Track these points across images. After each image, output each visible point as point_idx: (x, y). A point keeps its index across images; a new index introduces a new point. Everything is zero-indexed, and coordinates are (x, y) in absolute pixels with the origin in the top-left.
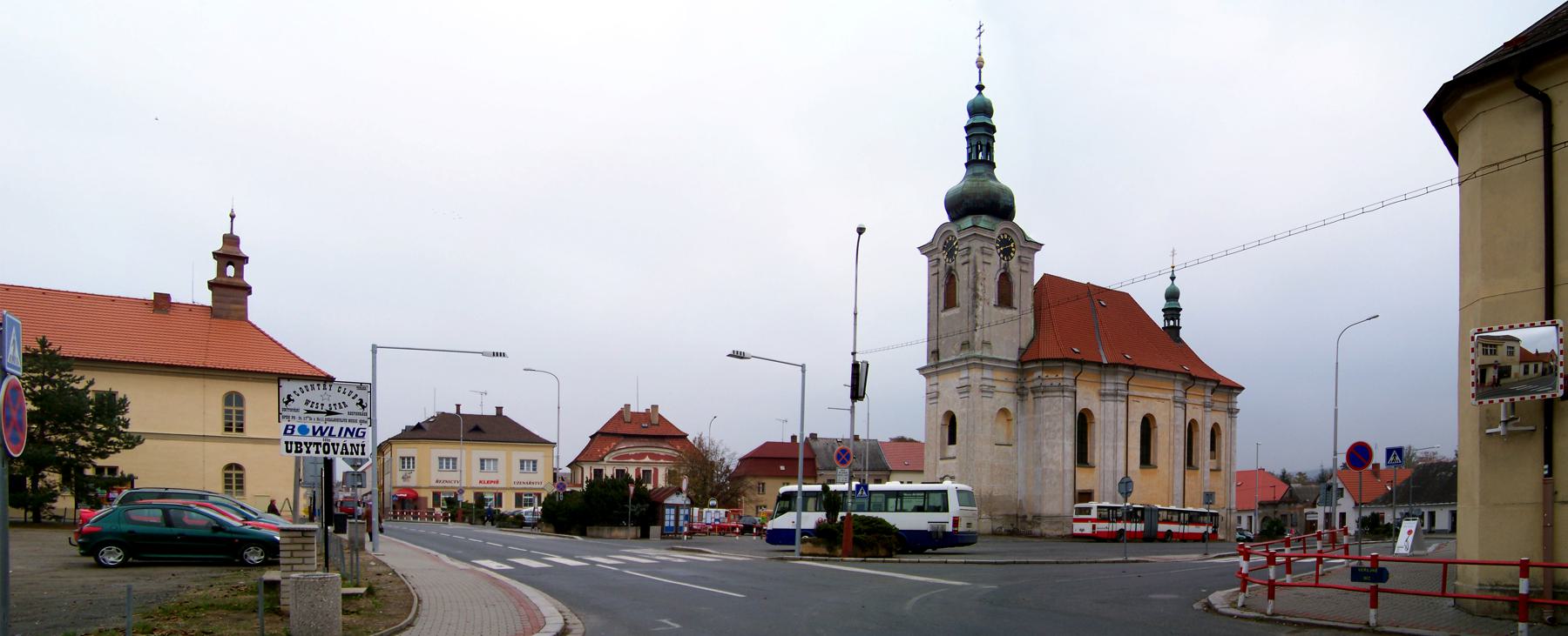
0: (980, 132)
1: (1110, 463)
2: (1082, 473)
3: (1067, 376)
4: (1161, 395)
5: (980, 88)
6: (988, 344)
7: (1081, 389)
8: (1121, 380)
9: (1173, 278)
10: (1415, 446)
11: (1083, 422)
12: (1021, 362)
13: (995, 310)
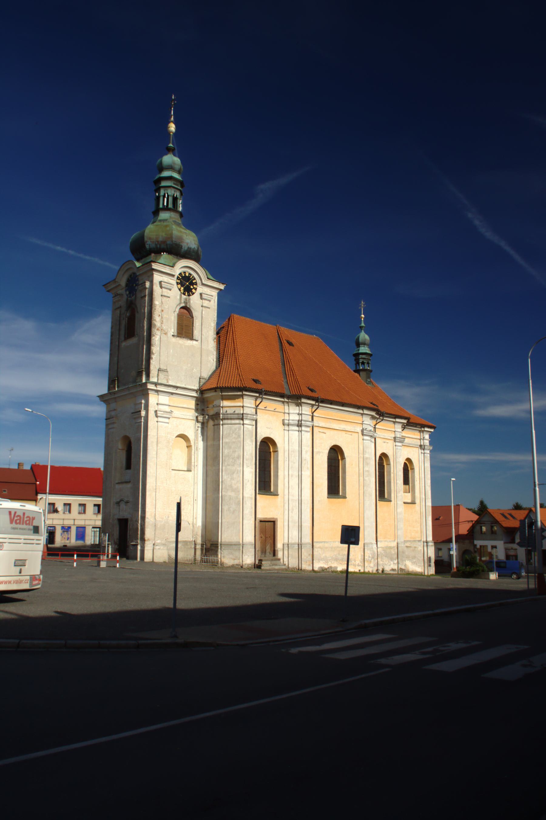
1: (295, 491)
2: (262, 499)
3: (248, 403)
4: (348, 427)
6: (166, 371)
7: (261, 417)
8: (306, 410)
10: (354, 360)
11: (266, 449)
12: (201, 391)
13: (174, 340)
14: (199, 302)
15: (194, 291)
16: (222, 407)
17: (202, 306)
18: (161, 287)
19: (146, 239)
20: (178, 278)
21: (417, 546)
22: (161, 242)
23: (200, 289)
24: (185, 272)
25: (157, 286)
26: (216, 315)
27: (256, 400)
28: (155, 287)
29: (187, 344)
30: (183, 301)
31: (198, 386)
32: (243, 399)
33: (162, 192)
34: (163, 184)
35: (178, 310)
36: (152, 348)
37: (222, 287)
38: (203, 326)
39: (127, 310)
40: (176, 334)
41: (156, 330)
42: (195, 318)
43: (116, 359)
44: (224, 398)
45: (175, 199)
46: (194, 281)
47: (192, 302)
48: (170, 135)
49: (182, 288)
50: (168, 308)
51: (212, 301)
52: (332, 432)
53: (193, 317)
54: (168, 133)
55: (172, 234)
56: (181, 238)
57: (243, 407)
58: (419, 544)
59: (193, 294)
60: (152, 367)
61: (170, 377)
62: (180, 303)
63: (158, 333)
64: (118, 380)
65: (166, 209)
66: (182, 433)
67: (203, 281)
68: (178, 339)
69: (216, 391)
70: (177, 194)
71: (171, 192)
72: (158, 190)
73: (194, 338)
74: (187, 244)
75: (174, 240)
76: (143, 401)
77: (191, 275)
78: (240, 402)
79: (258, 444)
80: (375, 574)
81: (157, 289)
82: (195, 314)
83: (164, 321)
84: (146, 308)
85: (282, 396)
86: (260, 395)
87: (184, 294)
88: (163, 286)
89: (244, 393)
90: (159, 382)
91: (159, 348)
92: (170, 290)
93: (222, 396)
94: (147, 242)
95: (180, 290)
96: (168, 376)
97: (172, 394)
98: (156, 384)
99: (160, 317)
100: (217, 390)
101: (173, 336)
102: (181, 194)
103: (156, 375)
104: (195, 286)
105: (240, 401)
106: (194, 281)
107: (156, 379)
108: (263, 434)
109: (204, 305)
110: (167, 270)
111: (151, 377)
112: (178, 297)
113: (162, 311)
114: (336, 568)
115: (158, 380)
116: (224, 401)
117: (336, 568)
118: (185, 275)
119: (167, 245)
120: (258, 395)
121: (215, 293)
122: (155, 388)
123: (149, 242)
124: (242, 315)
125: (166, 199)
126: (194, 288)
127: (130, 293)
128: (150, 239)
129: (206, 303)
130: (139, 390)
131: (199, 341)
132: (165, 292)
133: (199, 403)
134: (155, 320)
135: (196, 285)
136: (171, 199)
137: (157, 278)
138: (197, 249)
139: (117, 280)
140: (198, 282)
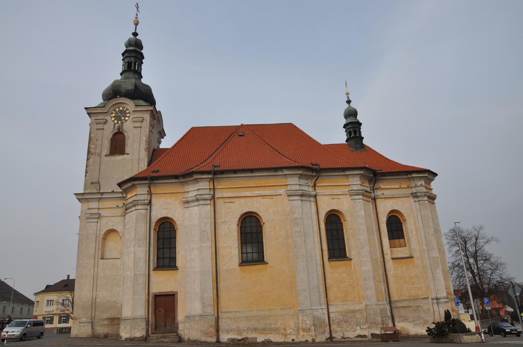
0: (134, 55)
5: (135, 34)
9: (349, 102)
13: (106, 158)
21: (422, 305)
52: (243, 200)
58: (425, 301)
74: (125, 88)
79: (153, 224)
80: (310, 343)
85: (176, 177)
108: (158, 213)
114: (256, 338)
117: (256, 338)
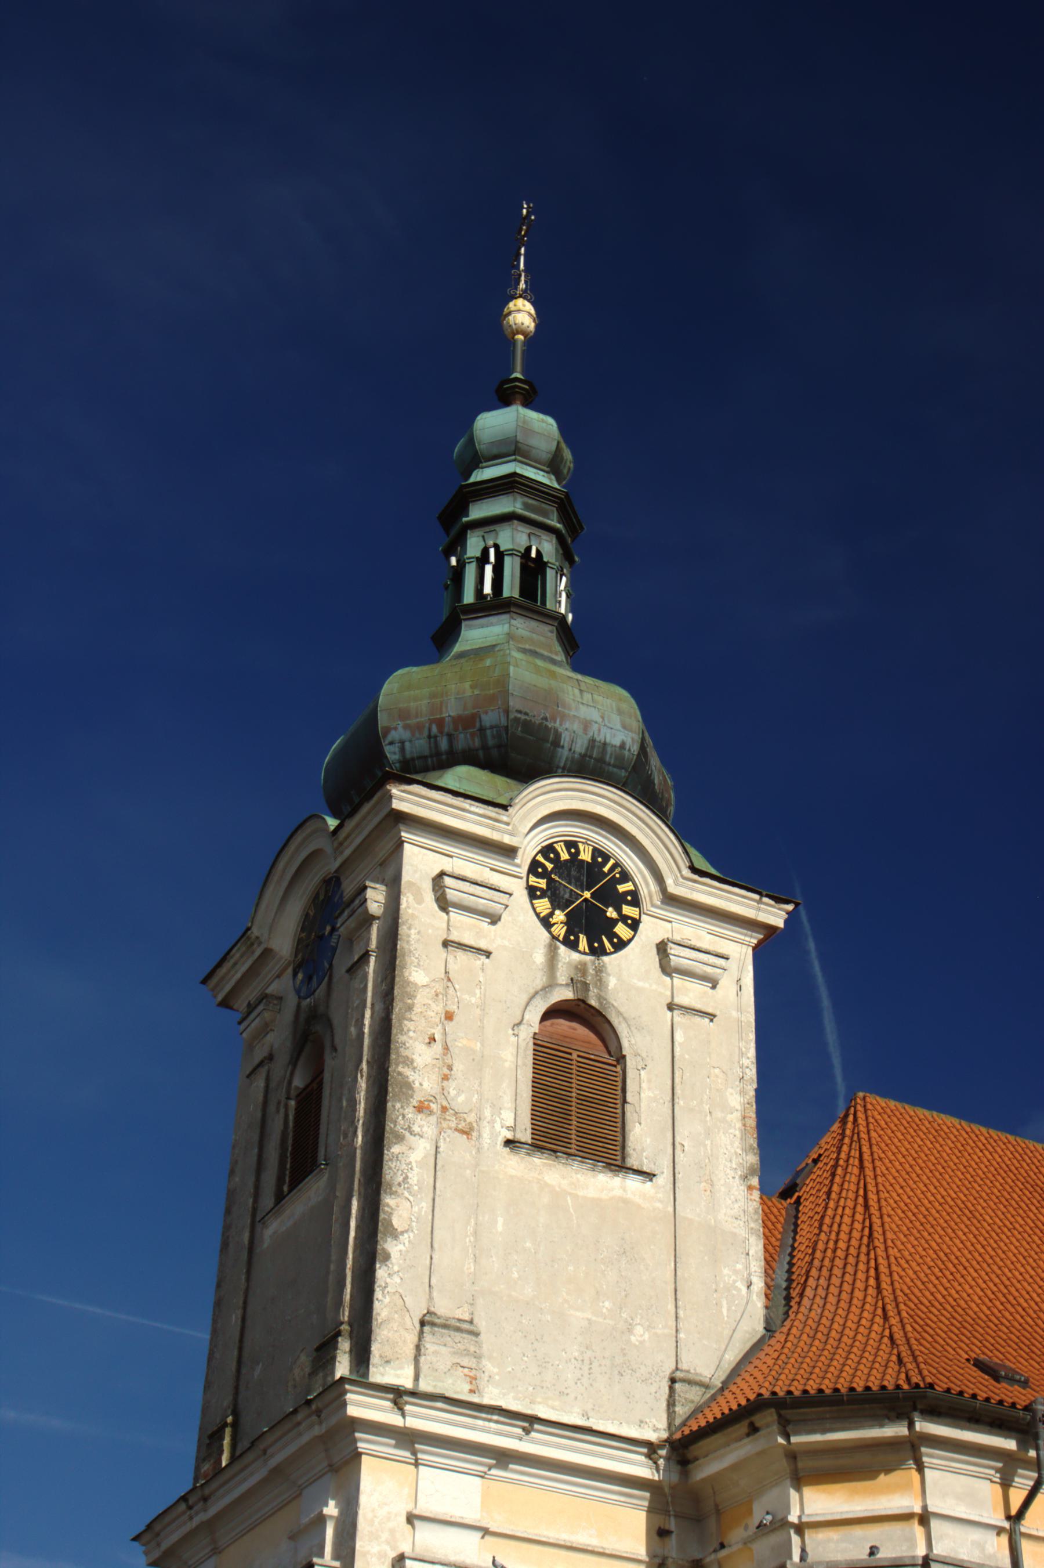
6: (467, 1328)
12: (682, 1448)
14: (660, 986)
15: (622, 930)
16: (800, 1529)
17: (671, 1007)
18: (444, 904)
19: (383, 720)
20: (534, 868)
22: (458, 720)
23: (655, 927)
24: (570, 845)
25: (420, 900)
26: (752, 1052)
27: (1006, 1484)
28: (407, 901)
29: (591, 1193)
30: (562, 978)
31: (663, 1424)
32: (920, 1468)
33: (474, 545)
34: (478, 511)
35: (534, 1016)
36: (388, 1201)
37: (775, 915)
38: (680, 1103)
39: (294, 1062)
40: (525, 1135)
41: (410, 1113)
42: (630, 1063)
43: (235, 1318)
44: (806, 1470)
45: (533, 570)
46: (622, 888)
47: (612, 982)
48: (514, 342)
49: (559, 916)
50: (483, 1006)
51: (727, 983)
53: (621, 1059)
54: (501, 336)
55: (503, 681)
56: (552, 699)
57: (924, 1518)
59: (620, 945)
60: (383, 1306)
61: (488, 1365)
62: (551, 985)
63: (425, 1125)
64: (235, 1425)
65: (492, 606)
66: (390, 1560)
67: (669, 881)
68: (539, 1161)
69: (754, 1429)
70: (547, 547)
71: (512, 538)
72: (457, 544)
73: (632, 1162)
74: (586, 725)
75: (514, 703)
76: (331, 1509)
77: (607, 858)
78: (904, 1488)
81: (419, 912)
82: (630, 1041)
83: (458, 1067)
84: (368, 1014)
86: (1023, 1445)
87: (573, 945)
88: (451, 895)
89: (923, 1426)
90: (424, 1386)
91: (425, 1205)
92: (494, 919)
93: (792, 1455)
94: (387, 731)
95: (546, 922)
96: (478, 1357)
97: (503, 1458)
98: (398, 1395)
99: (437, 1047)
100: (758, 1419)
101: (508, 1143)
102: (566, 553)
103: (410, 1350)
104: (627, 910)
105: (906, 1487)
106: (622, 888)
107: (410, 1371)
109: (680, 999)
110: (471, 819)
111: (375, 1358)
112: (540, 957)
113: (449, 1016)
115: (417, 1378)
116: (808, 1492)
118: (575, 856)
119: (482, 730)
120: (1010, 1444)
121: (739, 952)
122: (394, 1419)
123: (398, 733)
124: (914, 1103)
125: (489, 570)
126: (624, 919)
127: (309, 978)
128: (404, 715)
129: (691, 993)
130: (305, 1438)
131: (663, 1180)
132: (466, 928)
133: (672, 1525)
134: (409, 1062)
135: (636, 902)
136: (512, 567)
137: (420, 860)
138: (635, 749)
139: (255, 932)
140: (643, 892)
